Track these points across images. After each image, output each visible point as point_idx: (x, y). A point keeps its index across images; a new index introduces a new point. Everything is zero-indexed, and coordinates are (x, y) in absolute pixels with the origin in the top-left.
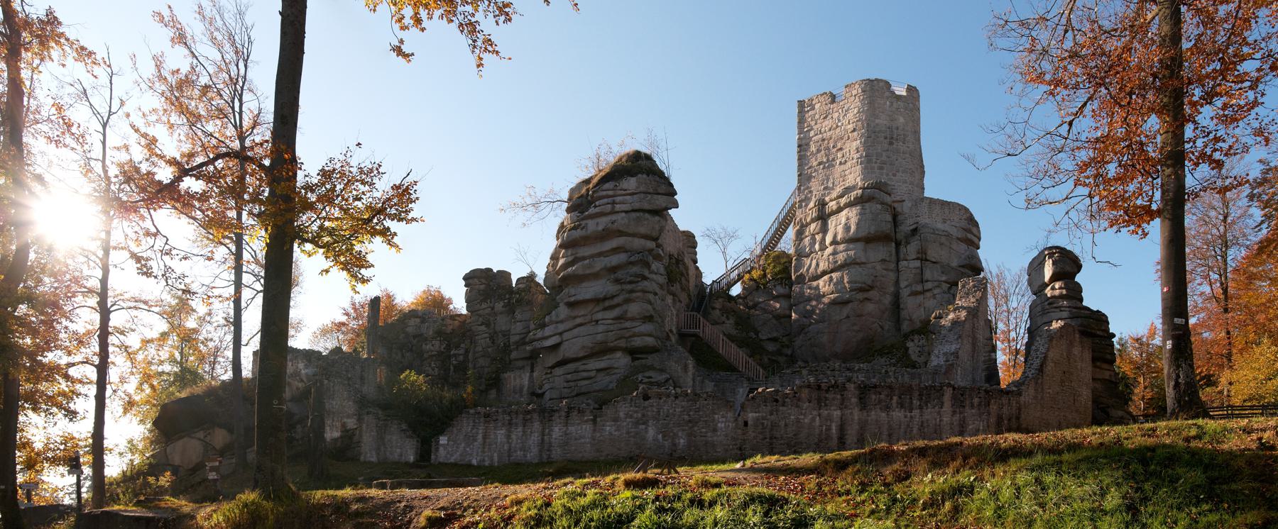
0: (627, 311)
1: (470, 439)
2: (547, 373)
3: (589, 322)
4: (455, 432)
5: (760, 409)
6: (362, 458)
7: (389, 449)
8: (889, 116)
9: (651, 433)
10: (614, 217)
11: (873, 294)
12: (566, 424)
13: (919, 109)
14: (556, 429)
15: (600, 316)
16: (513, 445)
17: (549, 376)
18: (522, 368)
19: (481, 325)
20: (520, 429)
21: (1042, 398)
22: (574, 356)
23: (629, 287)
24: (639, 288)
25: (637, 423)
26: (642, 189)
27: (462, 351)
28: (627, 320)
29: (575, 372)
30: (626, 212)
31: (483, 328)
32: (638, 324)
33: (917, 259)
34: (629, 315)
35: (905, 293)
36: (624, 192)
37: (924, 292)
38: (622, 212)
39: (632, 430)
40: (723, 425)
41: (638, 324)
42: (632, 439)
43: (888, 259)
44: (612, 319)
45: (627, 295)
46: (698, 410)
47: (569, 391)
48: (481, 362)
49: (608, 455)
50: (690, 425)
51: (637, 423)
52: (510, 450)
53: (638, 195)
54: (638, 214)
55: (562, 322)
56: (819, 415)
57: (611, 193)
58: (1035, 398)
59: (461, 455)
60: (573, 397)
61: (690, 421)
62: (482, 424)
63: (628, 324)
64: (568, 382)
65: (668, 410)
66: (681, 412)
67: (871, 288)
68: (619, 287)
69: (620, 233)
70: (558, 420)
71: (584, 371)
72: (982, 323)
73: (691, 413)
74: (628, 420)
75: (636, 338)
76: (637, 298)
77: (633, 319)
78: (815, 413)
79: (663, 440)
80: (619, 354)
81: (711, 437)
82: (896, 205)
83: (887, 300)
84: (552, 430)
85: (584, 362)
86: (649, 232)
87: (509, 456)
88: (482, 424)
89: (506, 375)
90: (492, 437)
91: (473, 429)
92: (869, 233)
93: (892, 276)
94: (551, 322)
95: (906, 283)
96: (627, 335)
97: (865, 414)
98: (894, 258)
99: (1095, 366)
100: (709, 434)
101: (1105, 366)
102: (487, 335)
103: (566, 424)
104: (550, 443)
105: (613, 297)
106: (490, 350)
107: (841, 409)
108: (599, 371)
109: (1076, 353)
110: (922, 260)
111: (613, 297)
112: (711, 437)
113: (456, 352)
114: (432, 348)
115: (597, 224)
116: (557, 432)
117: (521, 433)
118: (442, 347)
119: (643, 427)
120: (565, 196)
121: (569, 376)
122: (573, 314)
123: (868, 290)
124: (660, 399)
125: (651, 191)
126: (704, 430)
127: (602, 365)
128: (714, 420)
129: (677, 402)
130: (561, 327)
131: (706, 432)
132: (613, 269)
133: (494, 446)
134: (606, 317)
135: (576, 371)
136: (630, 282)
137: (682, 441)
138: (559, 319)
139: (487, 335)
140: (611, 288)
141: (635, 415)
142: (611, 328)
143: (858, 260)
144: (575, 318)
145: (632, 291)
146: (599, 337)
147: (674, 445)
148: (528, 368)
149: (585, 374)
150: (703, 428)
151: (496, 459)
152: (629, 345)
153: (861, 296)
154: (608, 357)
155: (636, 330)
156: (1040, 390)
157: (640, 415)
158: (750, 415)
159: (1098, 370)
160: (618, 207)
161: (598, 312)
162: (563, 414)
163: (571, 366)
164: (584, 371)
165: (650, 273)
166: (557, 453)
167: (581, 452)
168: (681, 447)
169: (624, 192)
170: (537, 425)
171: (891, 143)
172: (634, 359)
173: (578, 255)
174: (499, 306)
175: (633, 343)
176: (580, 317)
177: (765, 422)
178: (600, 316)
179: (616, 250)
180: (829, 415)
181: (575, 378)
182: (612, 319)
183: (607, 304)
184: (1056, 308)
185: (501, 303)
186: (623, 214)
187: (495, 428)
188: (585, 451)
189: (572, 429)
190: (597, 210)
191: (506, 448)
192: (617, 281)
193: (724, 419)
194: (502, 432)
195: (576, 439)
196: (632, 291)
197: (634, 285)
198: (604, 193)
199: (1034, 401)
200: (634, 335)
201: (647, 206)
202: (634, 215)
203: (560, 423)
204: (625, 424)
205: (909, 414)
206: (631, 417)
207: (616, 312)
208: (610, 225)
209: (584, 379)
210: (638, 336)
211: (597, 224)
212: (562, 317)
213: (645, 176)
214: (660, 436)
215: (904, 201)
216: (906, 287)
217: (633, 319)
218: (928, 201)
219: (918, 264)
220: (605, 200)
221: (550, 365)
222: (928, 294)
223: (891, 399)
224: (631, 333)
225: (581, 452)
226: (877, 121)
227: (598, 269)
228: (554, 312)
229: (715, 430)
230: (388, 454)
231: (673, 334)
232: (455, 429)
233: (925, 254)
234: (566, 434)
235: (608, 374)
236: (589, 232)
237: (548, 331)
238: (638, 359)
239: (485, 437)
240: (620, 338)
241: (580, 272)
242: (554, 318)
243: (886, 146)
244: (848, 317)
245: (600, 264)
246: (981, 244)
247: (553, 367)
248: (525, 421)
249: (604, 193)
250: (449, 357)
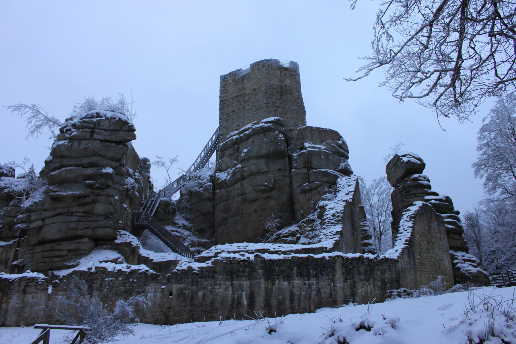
5: (183, 281)
8: (280, 79)
11: (275, 193)
13: (299, 74)
21: (414, 264)
22: (52, 237)
29: (50, 250)
33: (305, 167)
35: (297, 191)
37: (311, 190)
38: (97, 139)
43: (283, 168)
44: (82, 213)
56: (232, 285)
58: (409, 263)
67: (272, 189)
68: (90, 190)
72: (358, 209)
78: (228, 283)
80: (86, 240)
82: (287, 133)
83: (284, 197)
92: (270, 151)
93: (287, 180)
95: (297, 184)
97: (270, 283)
98: (288, 168)
99: (448, 237)
101: (456, 236)
107: (249, 279)
108: (69, 251)
109: (435, 226)
110: (308, 168)
120: (62, 121)
121: (46, 253)
123: (270, 191)
125: (118, 128)
135: (52, 250)
142: (82, 219)
143: (262, 170)
145: (99, 195)
149: (58, 253)
153: (264, 195)
156: (411, 256)
158: (174, 286)
159: (452, 240)
163: (48, 246)
164: (58, 250)
165: (113, 184)
171: (282, 95)
173: (63, 163)
177: (187, 292)
178: (74, 209)
180: (240, 285)
183: (80, 201)
184: (412, 194)
199: (408, 266)
205: (307, 282)
207: (87, 208)
210: (101, 228)
215: (292, 130)
216: (297, 187)
217: (99, 215)
218: (310, 129)
219: (305, 171)
221: (33, 243)
222: (314, 192)
223: (292, 269)
226: (272, 82)
233: (311, 164)
240: (88, 228)
243: (279, 97)
244: (256, 211)
246: (349, 155)
247: (34, 245)
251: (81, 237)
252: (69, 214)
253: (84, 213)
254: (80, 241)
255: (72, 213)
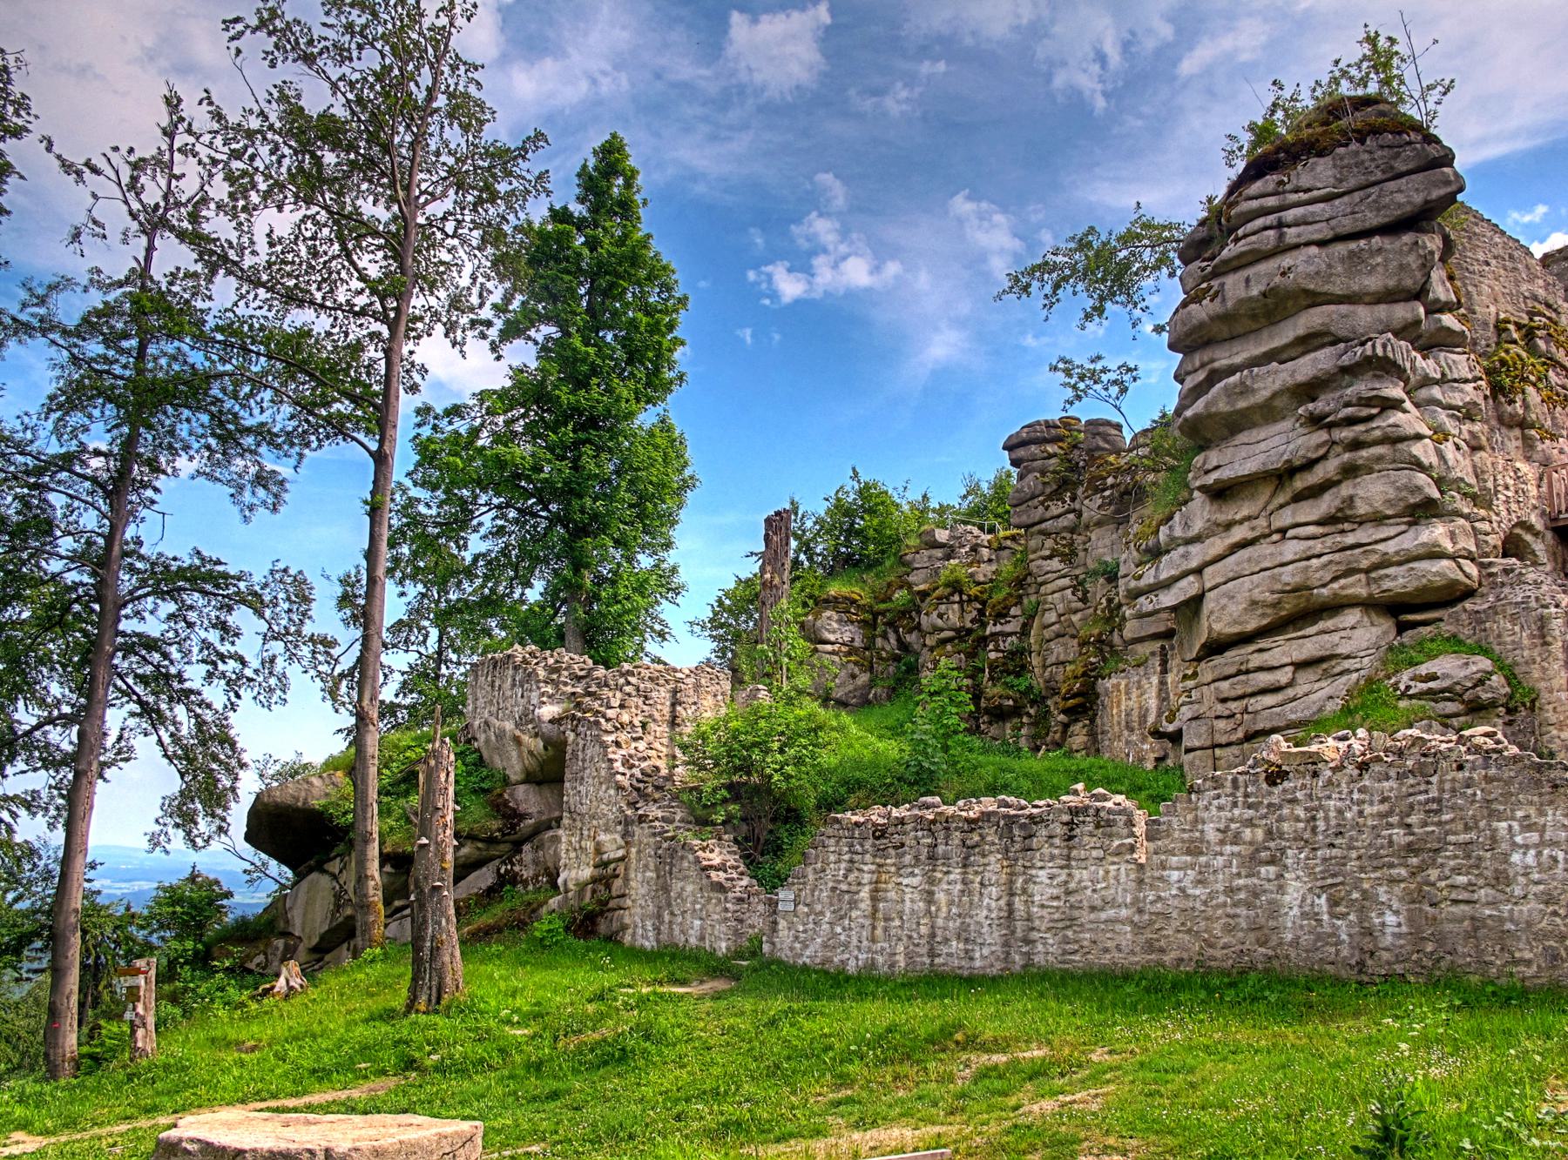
0: (1351, 498)
1: (844, 899)
2: (1185, 677)
3: (1265, 536)
4: (811, 877)
6: (627, 939)
7: (680, 919)
9: (1295, 892)
10: (1286, 261)
15: (1285, 518)
16: (940, 922)
17: (1190, 683)
19: (1050, 557)
20: (956, 875)
23: (1346, 434)
24: (1378, 433)
25: (1252, 861)
26: (1352, 183)
29: (1240, 672)
30: (1321, 244)
31: (1055, 564)
32: (1392, 531)
34: (1362, 509)
36: (1303, 196)
40: (1530, 859)
41: (1392, 531)
42: (1242, 911)
44: (1318, 523)
45: (1347, 456)
47: (1230, 725)
48: (1057, 650)
50: (1414, 861)
51: (1252, 861)
52: (933, 935)
53: (1346, 199)
54: (1353, 245)
57: (1271, 202)
59: (825, 946)
60: (1240, 742)
61: (1410, 849)
62: (868, 857)
63: (1362, 535)
64: (1224, 701)
65: (1340, 812)
68: (1322, 436)
69: (1315, 299)
70: (1046, 850)
71: (1260, 669)
73: (1413, 819)
74: (1228, 849)
75: (1391, 571)
76: (1380, 459)
77: (1378, 519)
79: (1333, 915)
80: (1352, 617)
85: (1263, 644)
86: (1391, 283)
87: (932, 954)
88: (868, 857)
89: (1109, 684)
90: (892, 895)
91: (849, 870)
96: (1365, 564)
102: (1066, 582)
105: (1310, 465)
106: (1075, 618)
108: (1300, 666)
111: (1310, 465)
113: (998, 628)
115: (1248, 280)
116: (1044, 882)
118: (968, 617)
119: (1272, 869)
121: (1225, 685)
122: (1222, 518)
124: (1315, 775)
126: (1462, 880)
127: (1308, 648)
130: (1197, 554)
132: (1308, 390)
134: (1302, 519)
136: (1351, 421)
137: (1390, 919)
138: (1191, 533)
139: (1066, 582)
140: (1306, 442)
141: (1247, 834)
142: (1318, 546)
144: (1229, 526)
146: (1289, 576)
148: (1156, 662)
149: (1264, 679)
150: (1457, 870)
151: (901, 961)
152: (1375, 590)
154: (1321, 625)
155: (1390, 547)
157: (1260, 834)
160: (1291, 234)
161: (1281, 506)
162: (1059, 830)
164: (1260, 669)
166: (1047, 950)
168: (1388, 940)
169: (1303, 196)
172: (1402, 628)
173: (1216, 365)
174: (1092, 507)
175: (1387, 584)
176: (1241, 522)
178: (1285, 518)
179: (1308, 342)
182: (1318, 523)
183: (1300, 483)
186: (1314, 250)
190: (1242, 247)
191: (924, 930)
192: (1316, 421)
193: (1534, 837)
194: (915, 881)
195: (1093, 909)
196: (1356, 445)
197: (1360, 428)
198: (1255, 204)
200: (1385, 563)
201: (1373, 219)
202: (1341, 249)
204: (1219, 861)
206: (1236, 840)
207: (1326, 504)
208: (1277, 279)
209: (1264, 691)
210: (1400, 564)
211: (1248, 280)
212: (1198, 526)
220: (1259, 222)
224: (1375, 558)
225: (1106, 950)
227: (1266, 394)
228: (1177, 517)
229: (1501, 879)
230: (677, 931)
231: (1536, 534)
232: (810, 869)
234: (1068, 893)
235: (1327, 675)
236: (1230, 304)
238: (1414, 625)
245: (1273, 380)
249: (1255, 204)
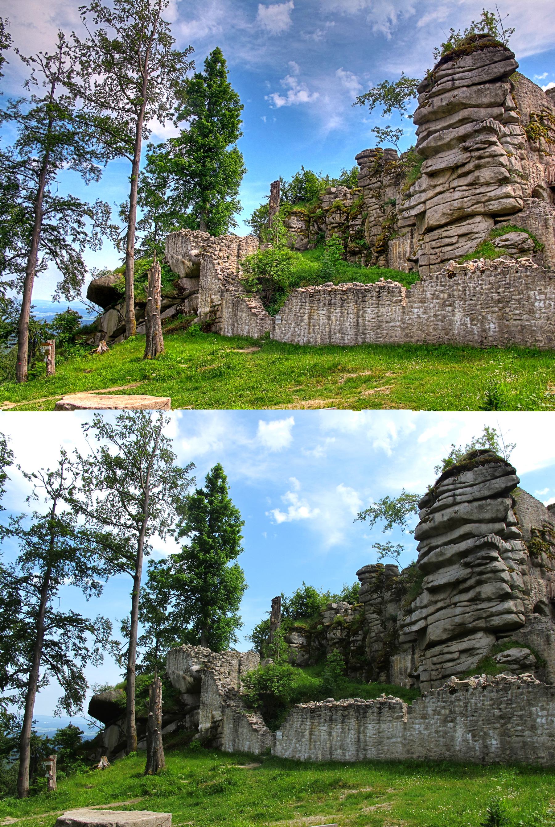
1: (299, 735)
12: (379, 721)
14: (370, 726)
18: (405, 651)
20: (339, 726)
22: (438, 639)
27: (359, 638)
28: (483, 600)
29: (440, 654)
38: (464, 502)
39: (441, 729)
45: (478, 577)
46: (510, 702)
49: (419, 757)
50: (502, 721)
52: (331, 748)
55: (425, 607)
62: (308, 720)
65: (476, 704)
66: (491, 705)
68: (469, 570)
70: (371, 717)
81: (530, 737)
84: (366, 728)
88: (308, 720)
94: (417, 608)
96: (485, 615)
100: (527, 733)
102: (378, 622)
103: (379, 721)
104: (365, 742)
112: (530, 737)
114: (334, 636)
117: (340, 730)
118: (344, 635)
126: (519, 728)
128: (531, 714)
129: (485, 693)
131: (522, 731)
133: (318, 743)
137: (494, 742)
139: (378, 622)
145: (481, 573)
147: (486, 747)
149: (449, 656)
163: (437, 649)
164: (446, 237)
167: (393, 753)
170: (353, 722)
178: (455, 184)
181: (440, 660)
183: (460, 171)
185: (390, 593)
187: (319, 723)
188: (397, 752)
189: (384, 726)
203: (374, 720)
210: (497, 615)
213: (480, 467)
214: (470, 736)
217: (489, 600)
228: (418, 599)
230: (240, 746)
236: (436, 523)
237: (415, 616)
239: (311, 734)
240: (479, 618)
241: (434, 560)
242: (418, 604)
248: (344, 717)
250: (349, 643)
251: (472, 215)
252: (453, 606)
253: (468, 601)
254: (470, 221)
255: (455, 604)
